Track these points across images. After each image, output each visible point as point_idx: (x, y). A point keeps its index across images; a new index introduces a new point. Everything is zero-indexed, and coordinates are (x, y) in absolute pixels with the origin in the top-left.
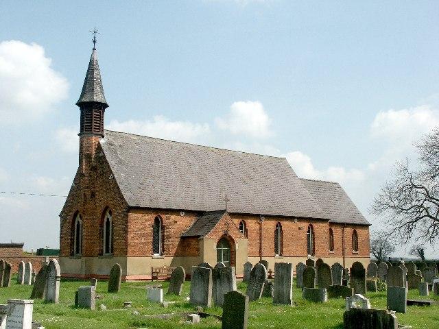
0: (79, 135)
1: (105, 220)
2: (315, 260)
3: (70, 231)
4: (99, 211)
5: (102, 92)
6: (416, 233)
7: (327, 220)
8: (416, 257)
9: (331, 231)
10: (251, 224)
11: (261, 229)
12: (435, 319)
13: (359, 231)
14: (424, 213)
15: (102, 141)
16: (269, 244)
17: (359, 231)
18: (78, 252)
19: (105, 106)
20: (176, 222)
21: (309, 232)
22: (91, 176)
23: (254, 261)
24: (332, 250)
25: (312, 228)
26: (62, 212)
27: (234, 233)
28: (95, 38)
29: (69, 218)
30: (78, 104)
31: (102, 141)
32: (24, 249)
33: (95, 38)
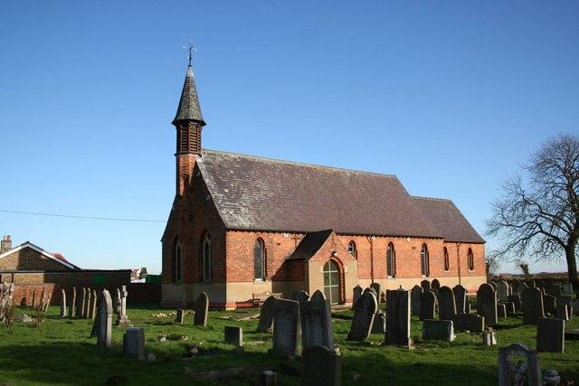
1: (177, 248)
2: (430, 280)
5: (199, 110)
6: (530, 249)
8: (520, 272)
9: (445, 249)
10: (362, 243)
11: (371, 249)
12: (578, 361)
14: (537, 229)
15: (199, 160)
16: (381, 264)
18: (179, 279)
19: (203, 124)
20: (279, 244)
21: (423, 251)
23: (365, 284)
24: (447, 269)
25: (426, 248)
27: (343, 255)
29: (171, 243)
30: (174, 123)
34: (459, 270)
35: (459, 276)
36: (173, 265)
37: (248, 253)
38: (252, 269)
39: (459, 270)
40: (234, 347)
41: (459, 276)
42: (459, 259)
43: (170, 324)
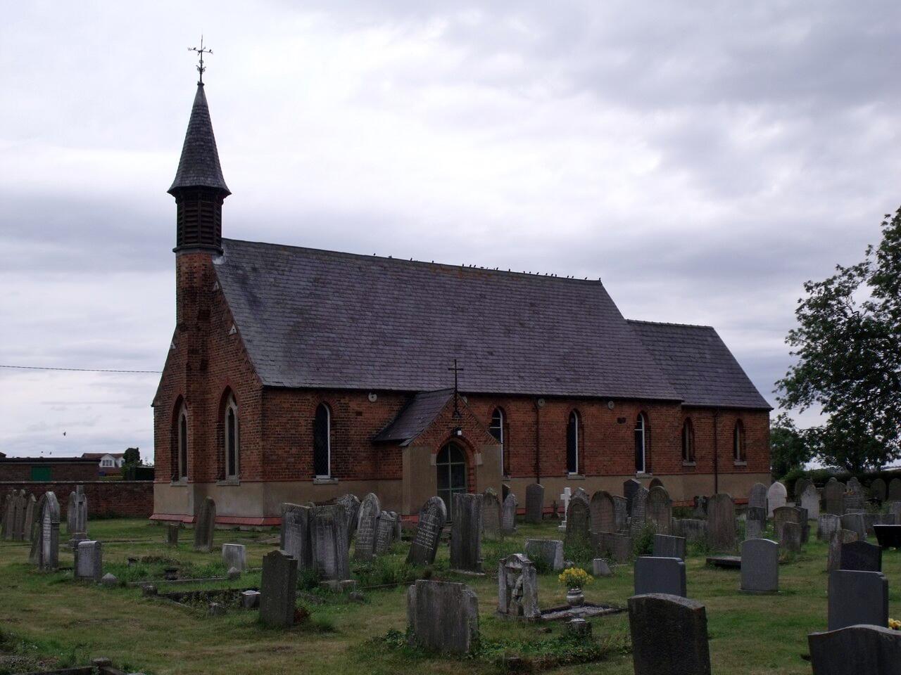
0: (175, 251)
3: (169, 436)
4: (216, 394)
7: (678, 402)
11: (537, 423)
13: (747, 419)
17: (747, 419)
20: (359, 414)
22: (199, 330)
26: (156, 399)
28: (201, 62)
29: (170, 412)
31: (218, 261)
32: (7, 457)
33: (201, 62)
34: (715, 461)
35: (716, 474)
36: (174, 450)
37: (303, 429)
38: (309, 459)
39: (715, 461)
40: (799, 544)
41: (716, 474)
42: (715, 440)
43: (501, 525)
